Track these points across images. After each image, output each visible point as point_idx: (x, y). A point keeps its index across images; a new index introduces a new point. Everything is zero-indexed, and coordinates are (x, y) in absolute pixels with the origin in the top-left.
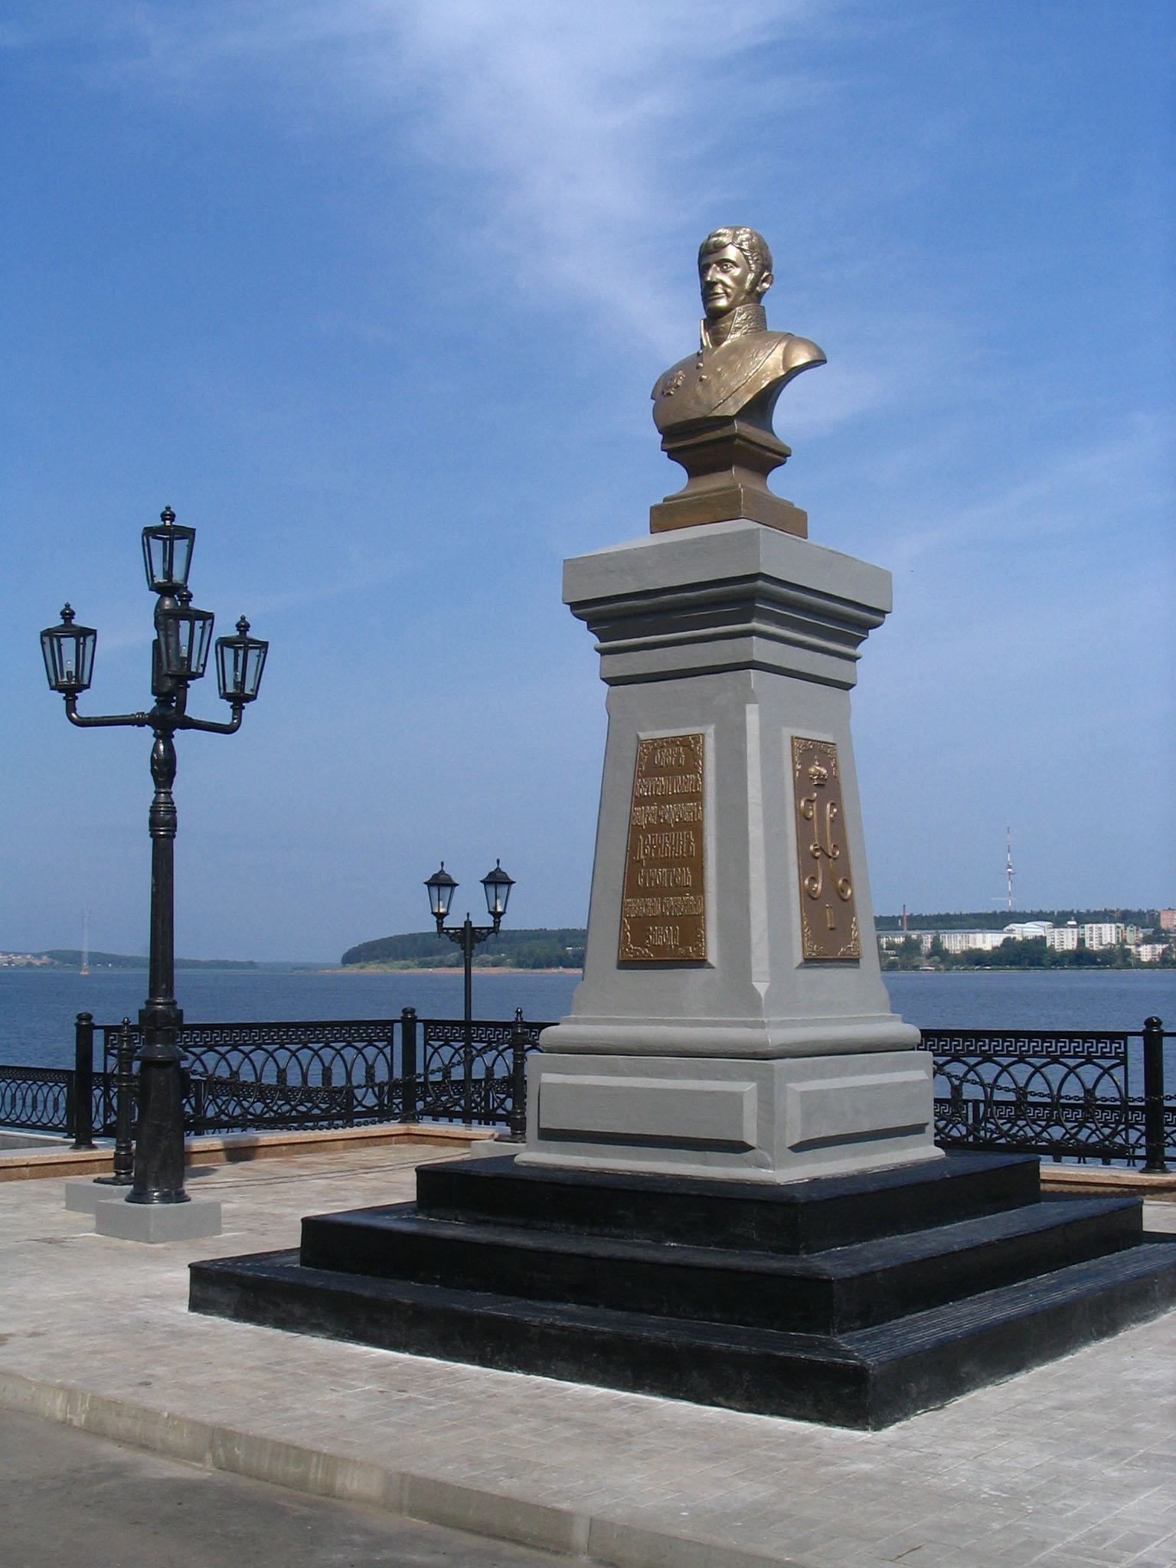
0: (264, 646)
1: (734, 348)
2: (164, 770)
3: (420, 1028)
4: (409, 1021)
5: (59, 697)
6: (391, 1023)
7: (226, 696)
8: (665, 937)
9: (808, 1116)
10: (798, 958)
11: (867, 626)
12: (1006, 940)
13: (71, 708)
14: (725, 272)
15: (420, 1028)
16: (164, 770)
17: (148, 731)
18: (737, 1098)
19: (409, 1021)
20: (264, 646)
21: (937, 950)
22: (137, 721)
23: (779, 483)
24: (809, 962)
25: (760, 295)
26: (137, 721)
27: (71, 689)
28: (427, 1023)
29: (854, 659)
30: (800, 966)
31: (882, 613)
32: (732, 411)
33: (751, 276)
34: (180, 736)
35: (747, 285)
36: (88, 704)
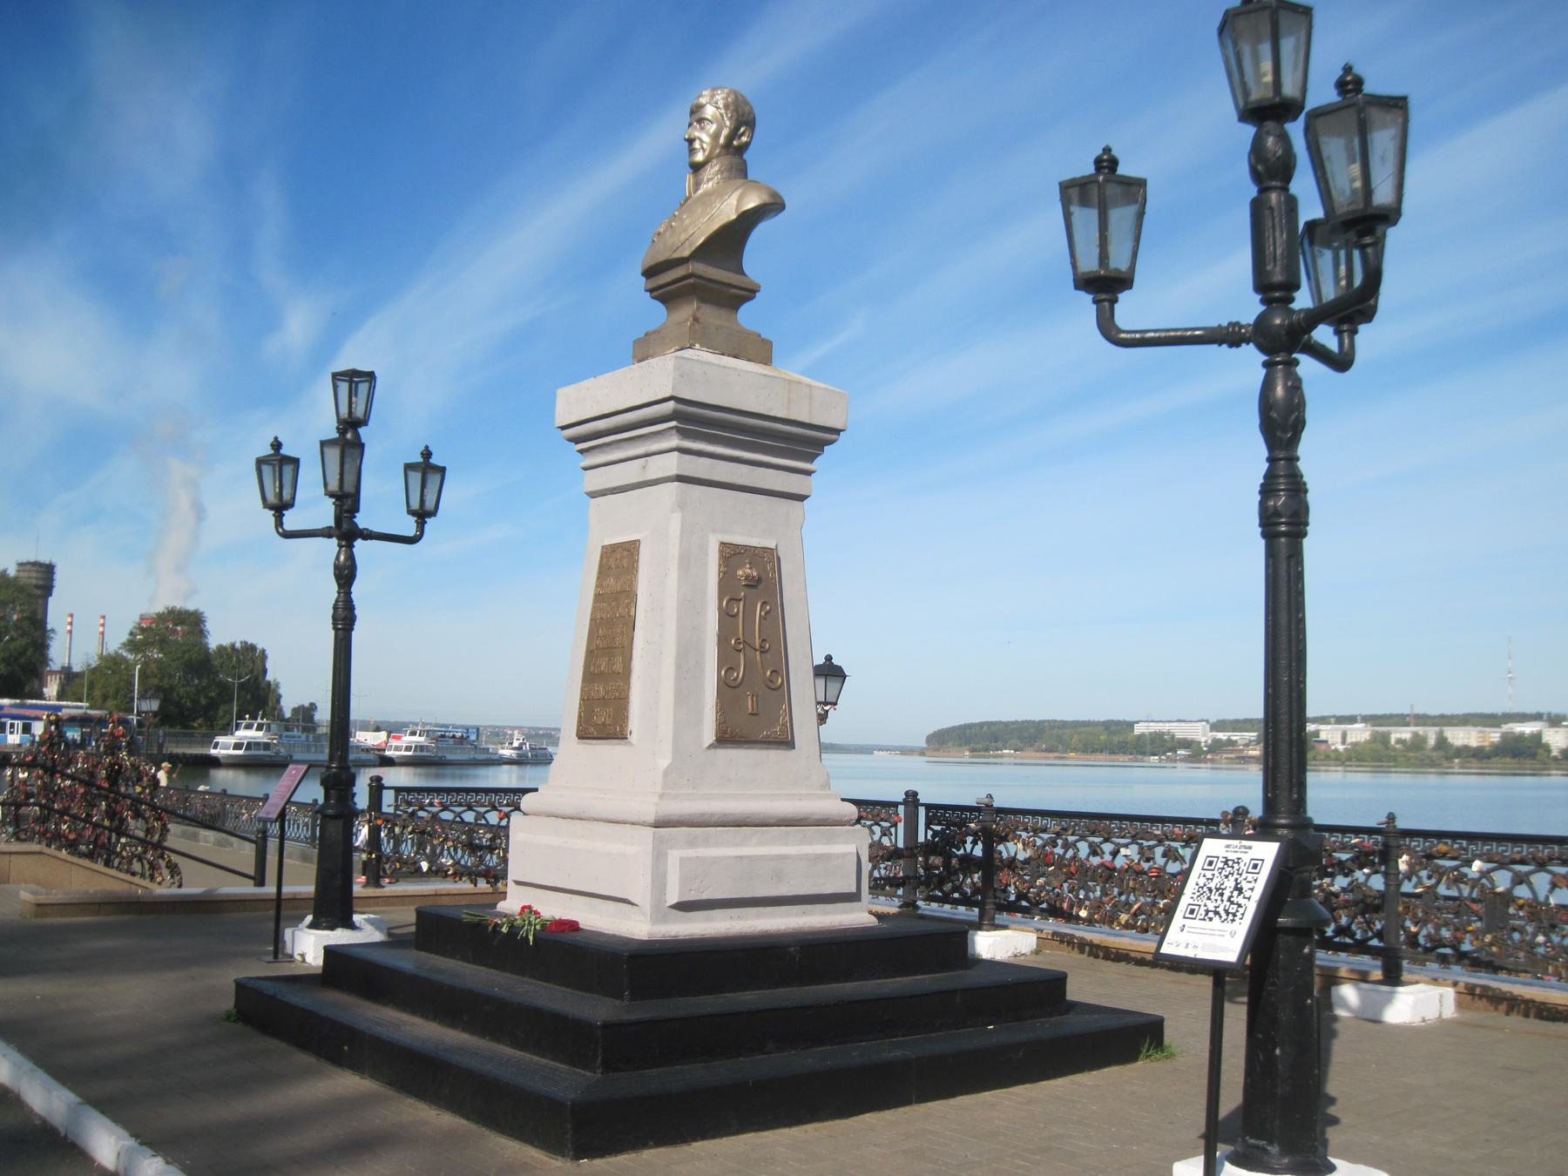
0: (442, 470)
1: (708, 194)
2: (345, 575)
3: (922, 811)
4: (912, 799)
5: (269, 515)
6: (895, 805)
7: (411, 512)
8: (601, 718)
9: (684, 881)
10: (709, 736)
11: (820, 445)
12: (1504, 736)
13: (279, 522)
14: (702, 129)
15: (922, 811)
16: (345, 575)
17: (333, 543)
18: (683, 861)
19: (912, 799)
20: (442, 470)
21: (1442, 742)
22: (1229, 337)
23: (747, 315)
24: (726, 738)
25: (743, 148)
26: (1229, 337)
27: (280, 508)
28: (929, 807)
29: (809, 473)
30: (710, 747)
31: (837, 432)
32: (686, 253)
33: (725, 132)
34: (359, 544)
35: (722, 140)
36: (1130, 311)
